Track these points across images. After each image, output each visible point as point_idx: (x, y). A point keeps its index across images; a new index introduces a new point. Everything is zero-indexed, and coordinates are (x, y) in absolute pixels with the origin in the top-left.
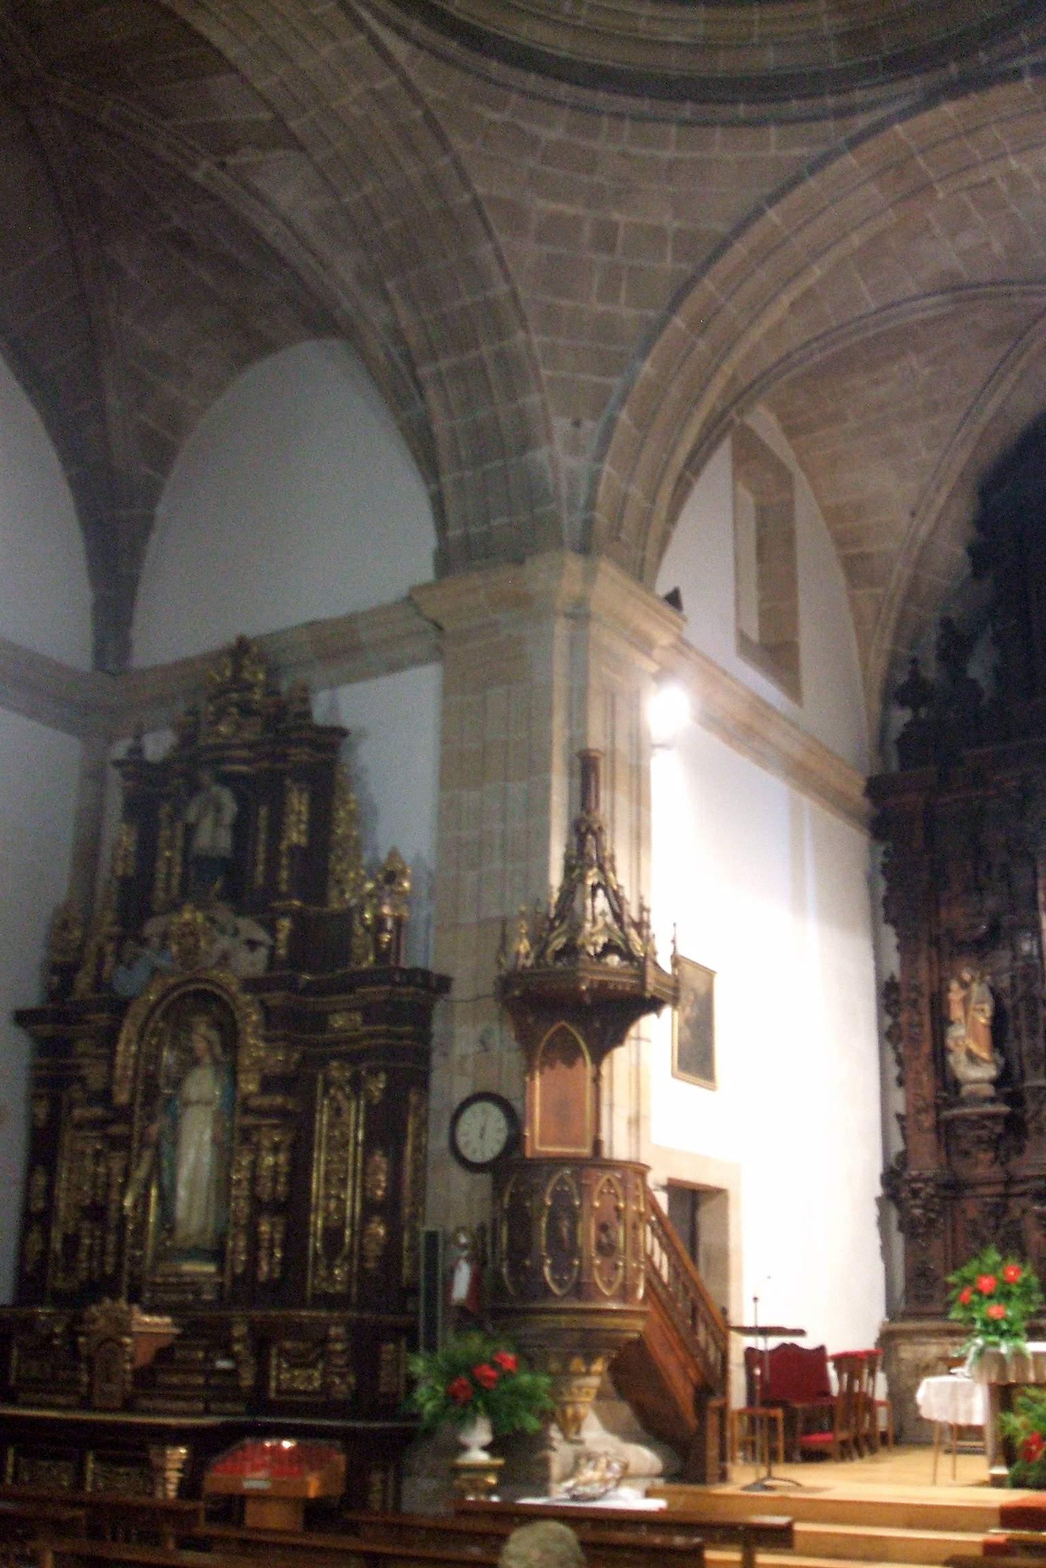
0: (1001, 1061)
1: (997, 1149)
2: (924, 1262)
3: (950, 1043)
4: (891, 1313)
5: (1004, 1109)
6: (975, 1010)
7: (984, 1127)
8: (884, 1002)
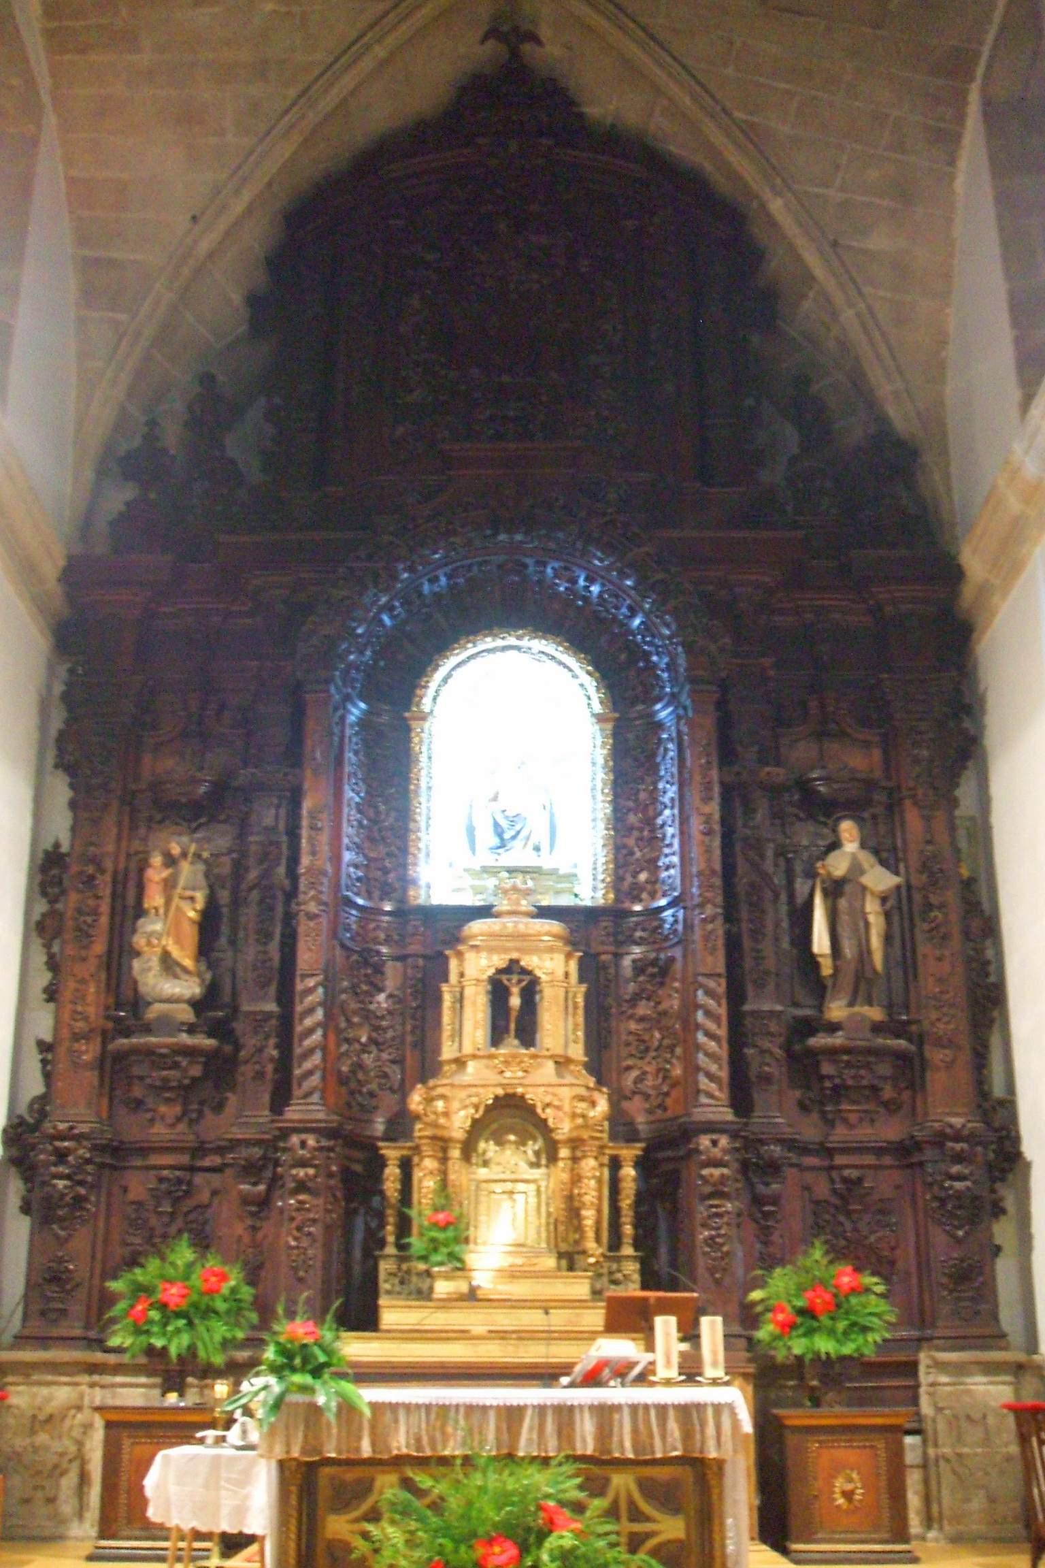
0: (208, 976)
1: (185, 1103)
2: (61, 1261)
3: (139, 941)
5: (205, 1042)
6: (182, 898)
7: (176, 1065)
8: (39, 878)
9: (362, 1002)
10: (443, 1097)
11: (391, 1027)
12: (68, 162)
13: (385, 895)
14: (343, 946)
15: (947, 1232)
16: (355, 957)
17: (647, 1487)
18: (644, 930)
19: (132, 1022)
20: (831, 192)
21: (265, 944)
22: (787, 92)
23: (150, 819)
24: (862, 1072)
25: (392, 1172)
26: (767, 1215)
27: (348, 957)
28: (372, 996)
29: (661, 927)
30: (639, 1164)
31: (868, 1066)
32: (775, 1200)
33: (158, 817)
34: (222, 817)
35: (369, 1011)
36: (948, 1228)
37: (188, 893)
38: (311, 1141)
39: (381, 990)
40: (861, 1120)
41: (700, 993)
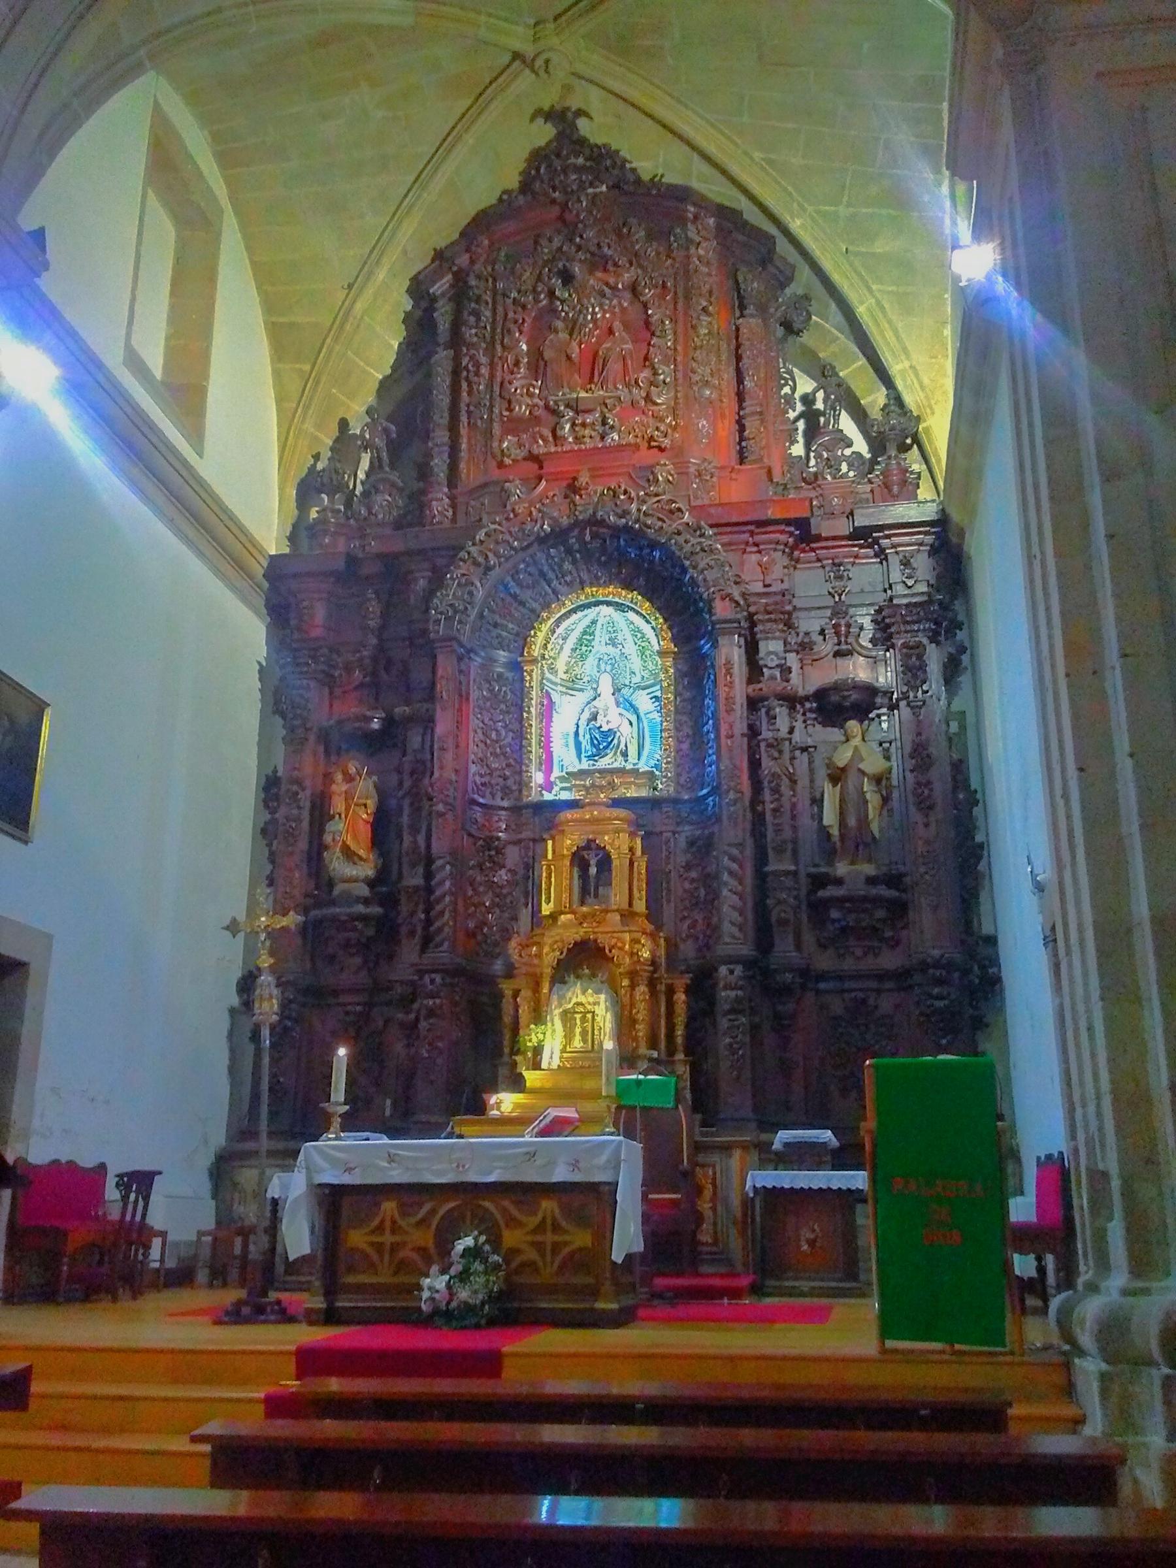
5: (376, 910)
6: (356, 805)
7: (355, 929)
14: (470, 835)
16: (481, 842)
17: (567, 1211)
24: (862, 916)
30: (688, 991)
31: (865, 911)
37: (363, 801)
38: (438, 978)
39: (504, 867)
40: (865, 954)
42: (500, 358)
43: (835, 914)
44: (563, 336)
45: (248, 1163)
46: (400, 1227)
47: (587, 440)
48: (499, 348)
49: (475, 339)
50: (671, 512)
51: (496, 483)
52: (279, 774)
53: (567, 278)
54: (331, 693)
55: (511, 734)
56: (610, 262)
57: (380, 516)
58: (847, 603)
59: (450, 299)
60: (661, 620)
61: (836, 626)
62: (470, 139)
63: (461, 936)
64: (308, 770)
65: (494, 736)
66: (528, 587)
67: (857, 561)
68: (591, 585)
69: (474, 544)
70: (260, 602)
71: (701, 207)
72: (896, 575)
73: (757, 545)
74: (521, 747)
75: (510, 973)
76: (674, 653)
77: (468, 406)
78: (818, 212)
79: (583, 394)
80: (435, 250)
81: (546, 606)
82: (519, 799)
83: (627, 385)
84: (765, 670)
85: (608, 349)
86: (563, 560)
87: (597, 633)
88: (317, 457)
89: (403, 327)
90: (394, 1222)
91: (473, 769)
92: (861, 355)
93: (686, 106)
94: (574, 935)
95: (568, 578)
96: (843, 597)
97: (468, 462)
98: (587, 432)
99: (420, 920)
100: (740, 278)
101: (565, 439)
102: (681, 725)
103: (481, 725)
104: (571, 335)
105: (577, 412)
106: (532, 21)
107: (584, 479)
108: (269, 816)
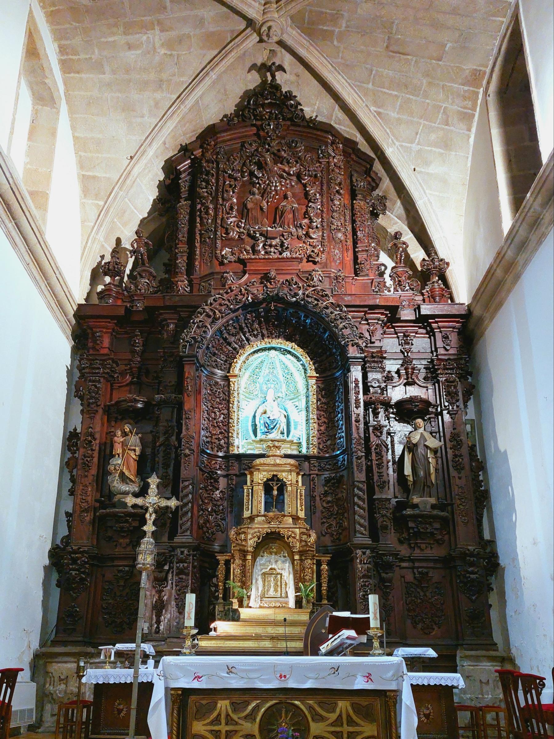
4: (43, 644)
9: (209, 494)
10: (244, 533)
11: (222, 505)
12: (73, 128)
13: (220, 448)
15: (468, 597)
17: (356, 708)
18: (330, 465)
19: (108, 502)
20: (414, 145)
21: (166, 469)
22: (396, 96)
23: (116, 418)
25: (221, 567)
26: (387, 587)
27: (203, 475)
28: (214, 492)
29: (337, 463)
31: (430, 524)
32: (390, 581)
33: (120, 417)
34: (148, 417)
35: (212, 497)
36: (468, 595)
39: (218, 489)
41: (356, 489)
42: (222, 205)
43: (411, 524)
44: (258, 197)
45: (56, 660)
46: (232, 719)
47: (272, 254)
48: (220, 200)
49: (206, 194)
50: (322, 296)
51: (218, 273)
52: (79, 430)
53: (261, 166)
54: (112, 386)
55: (222, 416)
56: (285, 160)
57: (143, 291)
58: (412, 357)
59: (189, 174)
60: (309, 359)
61: (406, 369)
62: (213, 75)
63: (195, 527)
64: (98, 428)
65: (213, 415)
66: (233, 335)
67: (417, 336)
68: (268, 337)
69: (206, 305)
70: (69, 333)
71: (336, 137)
72: (440, 344)
73: (367, 320)
74: (229, 423)
75: (224, 549)
76: (317, 377)
77: (200, 231)
78: (401, 146)
79: (269, 229)
80: (181, 145)
81: (242, 347)
82: (227, 451)
83: (296, 227)
84: (371, 388)
85: (285, 206)
86: (253, 321)
87: (263, 368)
88: (102, 257)
89: (157, 190)
90: (228, 715)
91: (203, 433)
92: (410, 232)
93: (339, 73)
94: (266, 528)
95: (255, 333)
96: (409, 354)
97: (200, 263)
98: (272, 250)
99: (169, 518)
100: (354, 180)
101: (260, 252)
102: (320, 417)
103: (207, 409)
104: (262, 196)
105: (266, 238)
106: (263, 2)
107: (273, 274)
108: (71, 455)
